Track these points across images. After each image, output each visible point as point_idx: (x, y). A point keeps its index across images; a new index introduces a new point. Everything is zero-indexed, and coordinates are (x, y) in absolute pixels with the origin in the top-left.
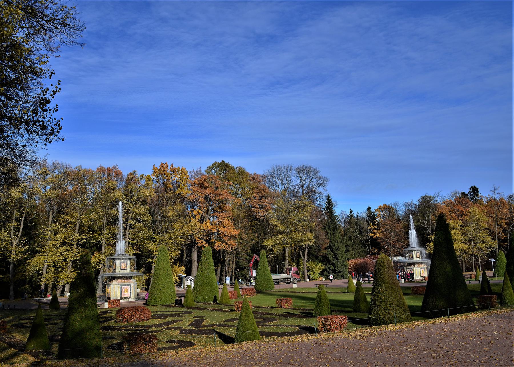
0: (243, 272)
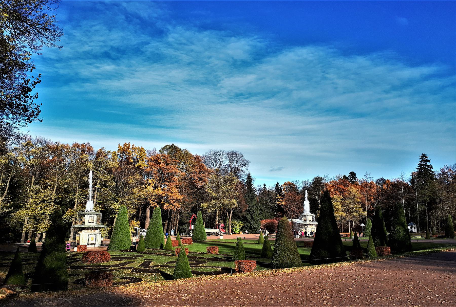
0: (184, 226)
